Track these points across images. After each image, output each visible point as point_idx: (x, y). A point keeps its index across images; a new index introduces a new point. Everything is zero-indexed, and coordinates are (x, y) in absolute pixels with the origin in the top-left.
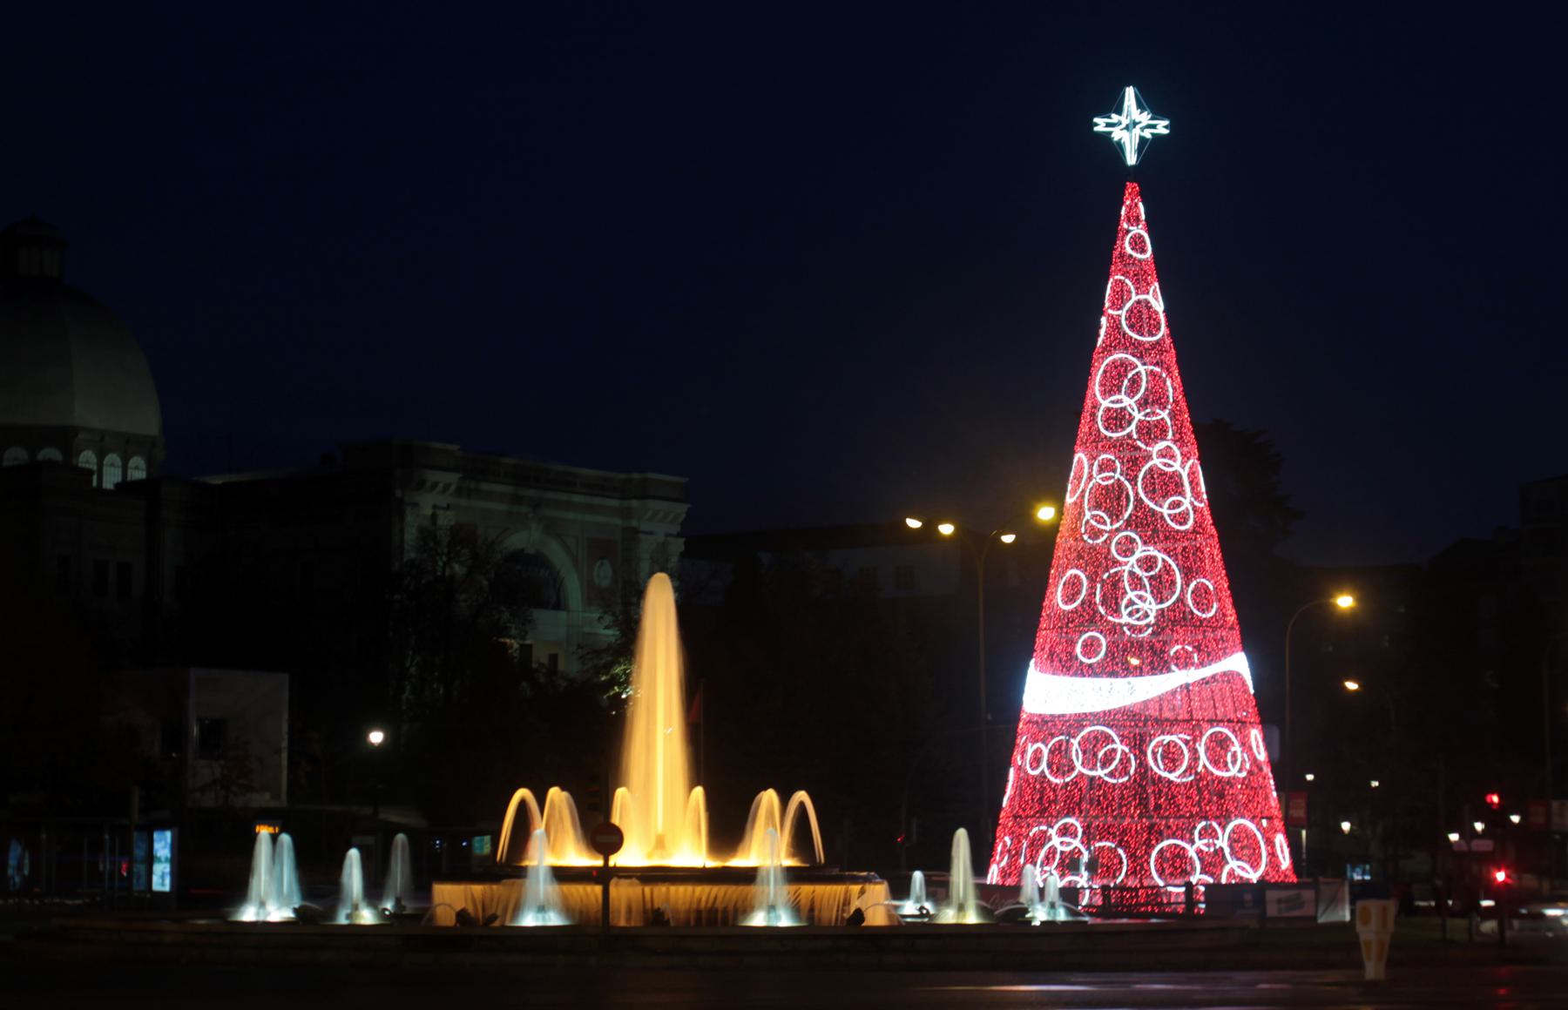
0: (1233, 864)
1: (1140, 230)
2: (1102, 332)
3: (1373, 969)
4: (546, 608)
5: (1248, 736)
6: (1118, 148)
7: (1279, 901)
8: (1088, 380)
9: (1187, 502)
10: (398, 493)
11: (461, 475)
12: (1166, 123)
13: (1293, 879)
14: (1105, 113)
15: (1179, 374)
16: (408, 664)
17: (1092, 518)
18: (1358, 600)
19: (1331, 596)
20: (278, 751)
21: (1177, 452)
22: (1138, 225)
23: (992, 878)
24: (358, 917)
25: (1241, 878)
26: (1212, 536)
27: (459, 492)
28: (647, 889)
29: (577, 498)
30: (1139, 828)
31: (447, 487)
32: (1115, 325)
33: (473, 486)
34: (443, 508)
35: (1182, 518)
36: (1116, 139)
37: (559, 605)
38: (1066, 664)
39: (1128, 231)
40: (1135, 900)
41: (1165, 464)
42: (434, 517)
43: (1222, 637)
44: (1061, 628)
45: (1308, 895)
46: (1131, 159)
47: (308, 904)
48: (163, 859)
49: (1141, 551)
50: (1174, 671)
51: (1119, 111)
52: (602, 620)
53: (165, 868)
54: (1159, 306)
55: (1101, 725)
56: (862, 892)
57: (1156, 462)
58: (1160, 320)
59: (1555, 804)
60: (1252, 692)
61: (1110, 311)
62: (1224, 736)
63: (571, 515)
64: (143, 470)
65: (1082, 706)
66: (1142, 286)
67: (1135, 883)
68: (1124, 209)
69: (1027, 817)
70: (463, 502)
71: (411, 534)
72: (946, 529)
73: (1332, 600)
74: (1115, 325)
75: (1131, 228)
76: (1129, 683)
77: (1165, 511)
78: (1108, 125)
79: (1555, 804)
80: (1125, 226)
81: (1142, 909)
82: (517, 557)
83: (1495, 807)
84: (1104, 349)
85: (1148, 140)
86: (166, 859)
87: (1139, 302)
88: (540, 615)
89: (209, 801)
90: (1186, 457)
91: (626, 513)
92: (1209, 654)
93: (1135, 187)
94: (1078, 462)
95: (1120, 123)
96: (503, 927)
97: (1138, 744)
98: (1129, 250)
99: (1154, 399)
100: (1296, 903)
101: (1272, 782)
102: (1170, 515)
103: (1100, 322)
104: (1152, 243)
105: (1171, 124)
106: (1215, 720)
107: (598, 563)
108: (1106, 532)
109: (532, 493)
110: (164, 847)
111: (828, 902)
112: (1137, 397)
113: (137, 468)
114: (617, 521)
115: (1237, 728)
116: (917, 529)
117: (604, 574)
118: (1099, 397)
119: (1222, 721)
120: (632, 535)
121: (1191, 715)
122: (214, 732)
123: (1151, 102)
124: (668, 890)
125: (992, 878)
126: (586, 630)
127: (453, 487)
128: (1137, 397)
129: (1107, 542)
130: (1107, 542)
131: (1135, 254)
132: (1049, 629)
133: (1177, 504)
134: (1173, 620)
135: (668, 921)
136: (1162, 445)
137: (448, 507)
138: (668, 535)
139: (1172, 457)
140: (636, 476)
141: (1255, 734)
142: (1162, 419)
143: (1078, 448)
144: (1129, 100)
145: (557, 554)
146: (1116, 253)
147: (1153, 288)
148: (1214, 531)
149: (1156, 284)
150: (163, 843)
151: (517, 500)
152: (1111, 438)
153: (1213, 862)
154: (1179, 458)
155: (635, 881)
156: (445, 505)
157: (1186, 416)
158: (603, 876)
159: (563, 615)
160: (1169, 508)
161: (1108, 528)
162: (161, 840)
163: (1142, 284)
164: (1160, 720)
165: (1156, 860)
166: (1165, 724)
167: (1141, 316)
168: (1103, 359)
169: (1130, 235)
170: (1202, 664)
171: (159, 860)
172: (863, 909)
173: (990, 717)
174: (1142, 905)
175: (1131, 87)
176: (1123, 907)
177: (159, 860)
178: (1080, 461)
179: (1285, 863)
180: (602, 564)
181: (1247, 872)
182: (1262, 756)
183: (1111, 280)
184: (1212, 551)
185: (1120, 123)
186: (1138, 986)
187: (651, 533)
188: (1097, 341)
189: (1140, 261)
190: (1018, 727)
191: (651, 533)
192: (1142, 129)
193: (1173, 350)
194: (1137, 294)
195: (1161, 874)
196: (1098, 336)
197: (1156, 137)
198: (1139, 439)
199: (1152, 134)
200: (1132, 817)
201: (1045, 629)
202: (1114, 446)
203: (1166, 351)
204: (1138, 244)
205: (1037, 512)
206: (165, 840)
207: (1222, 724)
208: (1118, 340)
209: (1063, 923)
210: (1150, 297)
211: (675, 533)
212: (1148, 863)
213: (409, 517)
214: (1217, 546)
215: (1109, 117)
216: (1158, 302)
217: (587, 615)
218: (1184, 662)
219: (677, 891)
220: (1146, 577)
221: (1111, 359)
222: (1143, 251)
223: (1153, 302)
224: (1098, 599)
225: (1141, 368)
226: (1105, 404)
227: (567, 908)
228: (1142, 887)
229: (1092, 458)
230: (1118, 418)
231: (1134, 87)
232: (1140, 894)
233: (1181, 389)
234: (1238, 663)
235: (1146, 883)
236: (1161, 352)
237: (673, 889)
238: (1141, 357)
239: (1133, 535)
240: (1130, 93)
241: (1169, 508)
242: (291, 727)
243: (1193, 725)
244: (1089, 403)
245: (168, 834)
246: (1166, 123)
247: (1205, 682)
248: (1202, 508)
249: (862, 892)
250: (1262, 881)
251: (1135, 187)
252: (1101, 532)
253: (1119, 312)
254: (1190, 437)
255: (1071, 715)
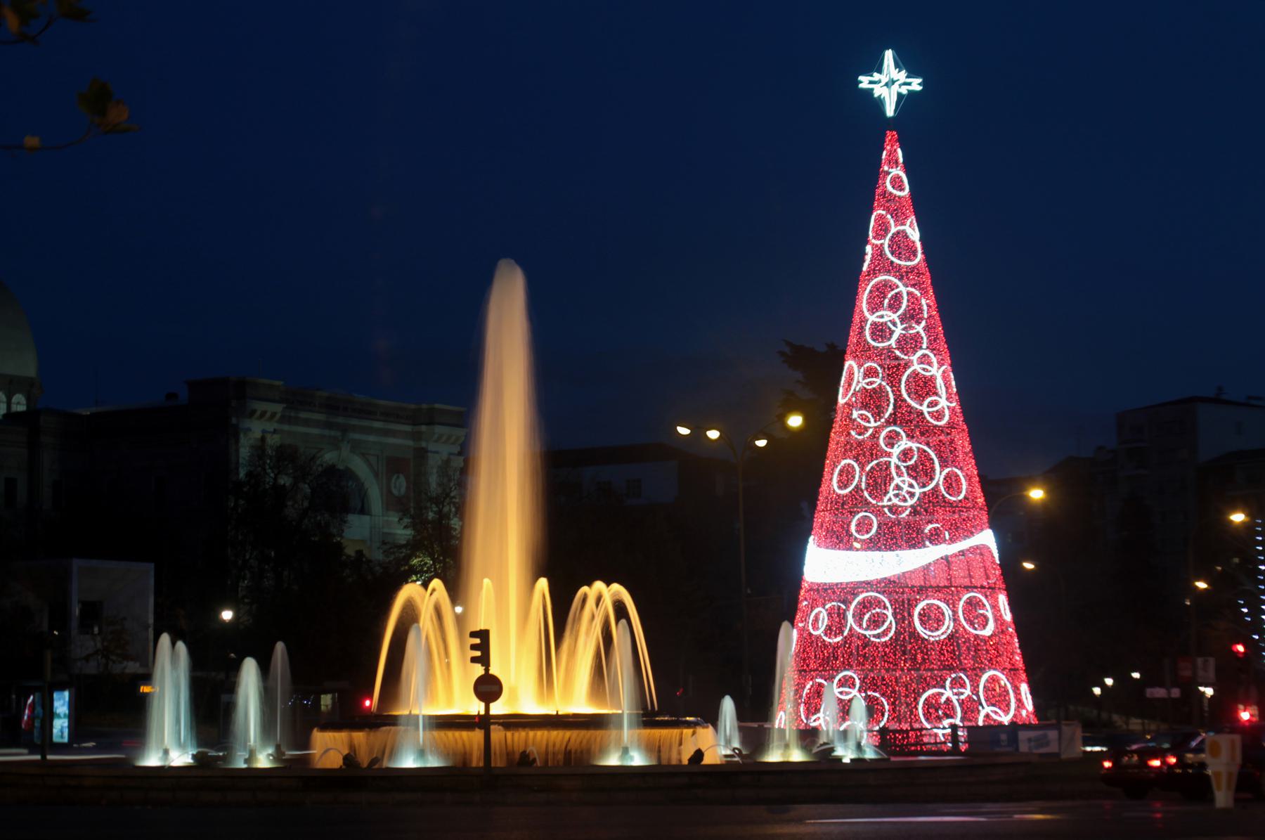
0: (986, 709)
1: (898, 172)
2: (868, 258)
3: (1222, 798)
4: (354, 513)
5: (997, 600)
6: (879, 104)
7: (1030, 740)
8: (855, 299)
9: (943, 403)
10: (234, 421)
11: (285, 405)
12: (920, 80)
13: (1034, 721)
14: (868, 72)
15: (934, 292)
16: (248, 557)
17: (859, 417)
18: (1048, 492)
19: (1026, 490)
20: (147, 627)
21: (934, 360)
22: (897, 167)
23: (780, 723)
24: (256, 760)
25: (995, 721)
26: (963, 430)
27: (284, 419)
28: (509, 734)
29: (377, 425)
30: (908, 679)
31: (273, 415)
32: (879, 251)
33: (293, 414)
34: (270, 432)
35: (939, 415)
36: (876, 95)
37: (363, 510)
38: (840, 539)
39: (888, 173)
40: (906, 740)
41: (924, 369)
42: (263, 439)
43: (974, 516)
44: (837, 509)
45: (1052, 734)
46: (890, 111)
47: (200, 750)
48: (62, 715)
49: (904, 443)
50: (928, 547)
51: (880, 71)
52: (401, 522)
53: (64, 723)
54: (915, 235)
55: (873, 591)
56: (694, 733)
57: (916, 367)
58: (916, 248)
59: (1200, 661)
60: (998, 562)
61: (874, 241)
62: (978, 600)
63: (372, 438)
64: (23, 405)
65: (857, 575)
66: (900, 220)
67: (906, 726)
68: (885, 153)
69: (811, 670)
70: (286, 427)
71: (244, 452)
72: (713, 434)
73: (1025, 493)
74: (879, 251)
75: (890, 170)
76: (897, 556)
77: (925, 409)
78: (871, 82)
79: (1200, 661)
80: (886, 168)
81: (913, 748)
82: (331, 470)
83: (1241, 656)
84: (869, 273)
85: (904, 95)
86: (65, 715)
87: (898, 232)
88: (353, 518)
89: (91, 668)
90: (941, 364)
91: (417, 436)
92: (959, 530)
93: (894, 135)
94: (848, 368)
95: (879, 82)
96: (381, 769)
97: (903, 610)
98: (890, 188)
99: (912, 316)
100: (1042, 742)
101: (1016, 640)
102: (929, 413)
103: (865, 250)
104: (909, 183)
105: (923, 81)
106: (970, 587)
107: (395, 477)
108: (870, 428)
109: (340, 420)
110: (63, 705)
111: (660, 740)
112: (900, 312)
113: (18, 403)
114: (410, 443)
115: (988, 593)
116: (687, 435)
117: (400, 485)
118: (867, 314)
119: (976, 587)
120: (421, 454)
121: (951, 583)
122: (92, 612)
123: (906, 62)
124: (527, 735)
125: (780, 723)
126: (386, 530)
127: (278, 416)
128: (900, 312)
129: (875, 436)
130: (875, 436)
131: (895, 192)
132: (827, 510)
133: (933, 404)
134: (931, 502)
135: (534, 760)
136: (919, 353)
137: (275, 431)
138: (451, 454)
139: (930, 364)
140: (424, 406)
141: (1002, 599)
142: (918, 333)
143: (848, 356)
144: (888, 60)
145: (360, 467)
146: (879, 191)
147: (910, 220)
148: (965, 427)
149: (913, 217)
150: (62, 702)
151: (329, 425)
152: (878, 347)
153: (970, 708)
154: (936, 365)
155: (500, 727)
156: (272, 430)
157: (940, 329)
158: (483, 722)
159: (366, 518)
160: (928, 406)
161: (873, 424)
162: (60, 699)
163: (900, 218)
164: (925, 587)
165: (924, 707)
166: (923, 590)
167: (901, 245)
168: (869, 281)
169: (890, 176)
170: (953, 540)
171: (59, 716)
172: (703, 750)
173: (749, 591)
174: (913, 745)
175: (890, 50)
176: (897, 746)
177: (59, 716)
178: (851, 367)
179: (1029, 705)
180: (398, 477)
181: (1000, 716)
182: (1008, 617)
183: (875, 213)
184: (963, 442)
185: (879, 82)
186: (1016, 816)
187: (437, 452)
188: (863, 266)
189: (899, 197)
190: (799, 594)
191: (437, 452)
192: (900, 86)
193: (928, 273)
194: (896, 225)
195: (927, 719)
196: (864, 261)
197: (911, 93)
198: (898, 349)
199: (908, 90)
200: (902, 670)
201: (823, 511)
202: (880, 352)
203: (923, 274)
204: (897, 183)
205: (787, 420)
206: (64, 699)
207: (975, 590)
208: (881, 264)
209: (871, 760)
210: (907, 228)
211: (456, 452)
212: (917, 709)
213: (243, 440)
214: (968, 439)
215: (872, 76)
216: (914, 229)
217: (386, 518)
218: (936, 538)
219: (535, 736)
220: (905, 467)
221: (876, 280)
222: (902, 189)
223: (909, 231)
224: (863, 486)
225: (903, 289)
226: (872, 318)
227: (444, 752)
228: (912, 729)
229: (860, 366)
230: (881, 331)
231: (892, 50)
232: (910, 735)
233: (936, 305)
234: (987, 538)
235: (917, 726)
236: (919, 274)
237: (531, 733)
238: (901, 279)
239: (898, 429)
240: (889, 55)
241: (928, 406)
242: (156, 605)
243: (949, 591)
244: (857, 319)
245: (66, 694)
246: (920, 80)
247: (962, 553)
248: (954, 407)
249: (694, 733)
250: (1013, 723)
251: (894, 135)
252: (866, 429)
253: (882, 241)
254: (943, 346)
255: (847, 584)
